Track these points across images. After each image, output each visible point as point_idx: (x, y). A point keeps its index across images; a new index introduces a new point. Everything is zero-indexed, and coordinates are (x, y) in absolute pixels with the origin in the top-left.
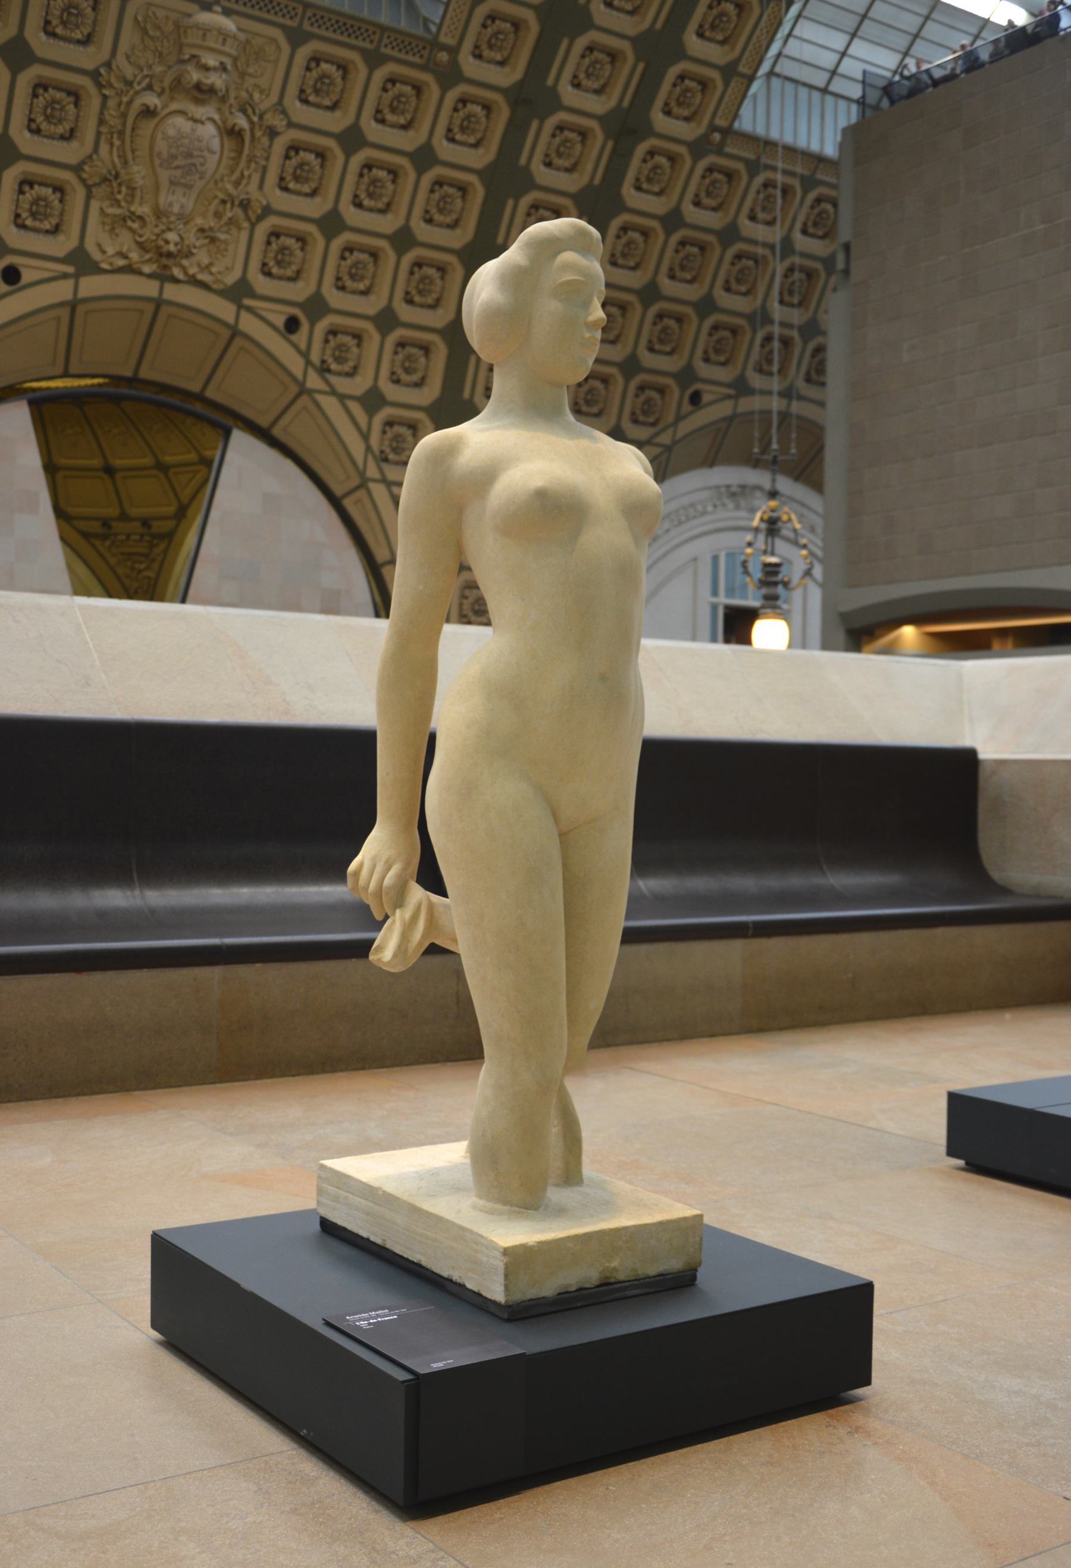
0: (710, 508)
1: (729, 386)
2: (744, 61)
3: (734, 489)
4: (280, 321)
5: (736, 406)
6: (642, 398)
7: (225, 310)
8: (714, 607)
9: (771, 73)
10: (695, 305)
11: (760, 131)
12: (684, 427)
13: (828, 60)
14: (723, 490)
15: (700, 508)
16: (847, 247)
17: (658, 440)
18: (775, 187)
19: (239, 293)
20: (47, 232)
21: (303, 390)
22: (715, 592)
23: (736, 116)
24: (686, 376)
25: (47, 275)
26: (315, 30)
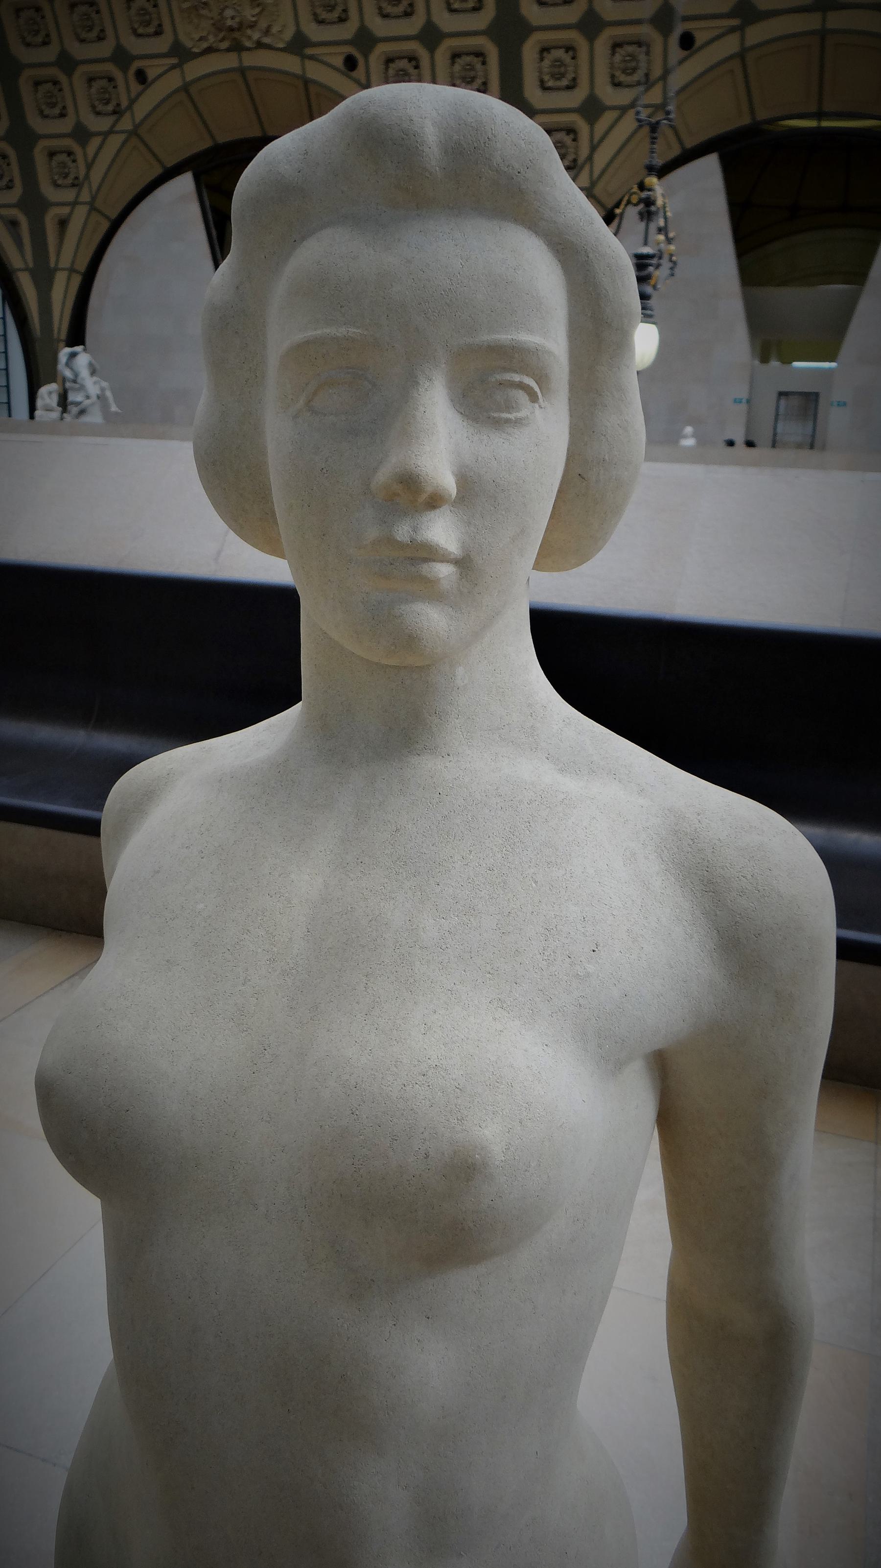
4: (339, 61)
5: (743, 39)
7: (290, 63)
12: (142, 109)
17: (118, 128)
19: (299, 45)
21: (134, 133)
24: (121, 58)
25: (716, 33)
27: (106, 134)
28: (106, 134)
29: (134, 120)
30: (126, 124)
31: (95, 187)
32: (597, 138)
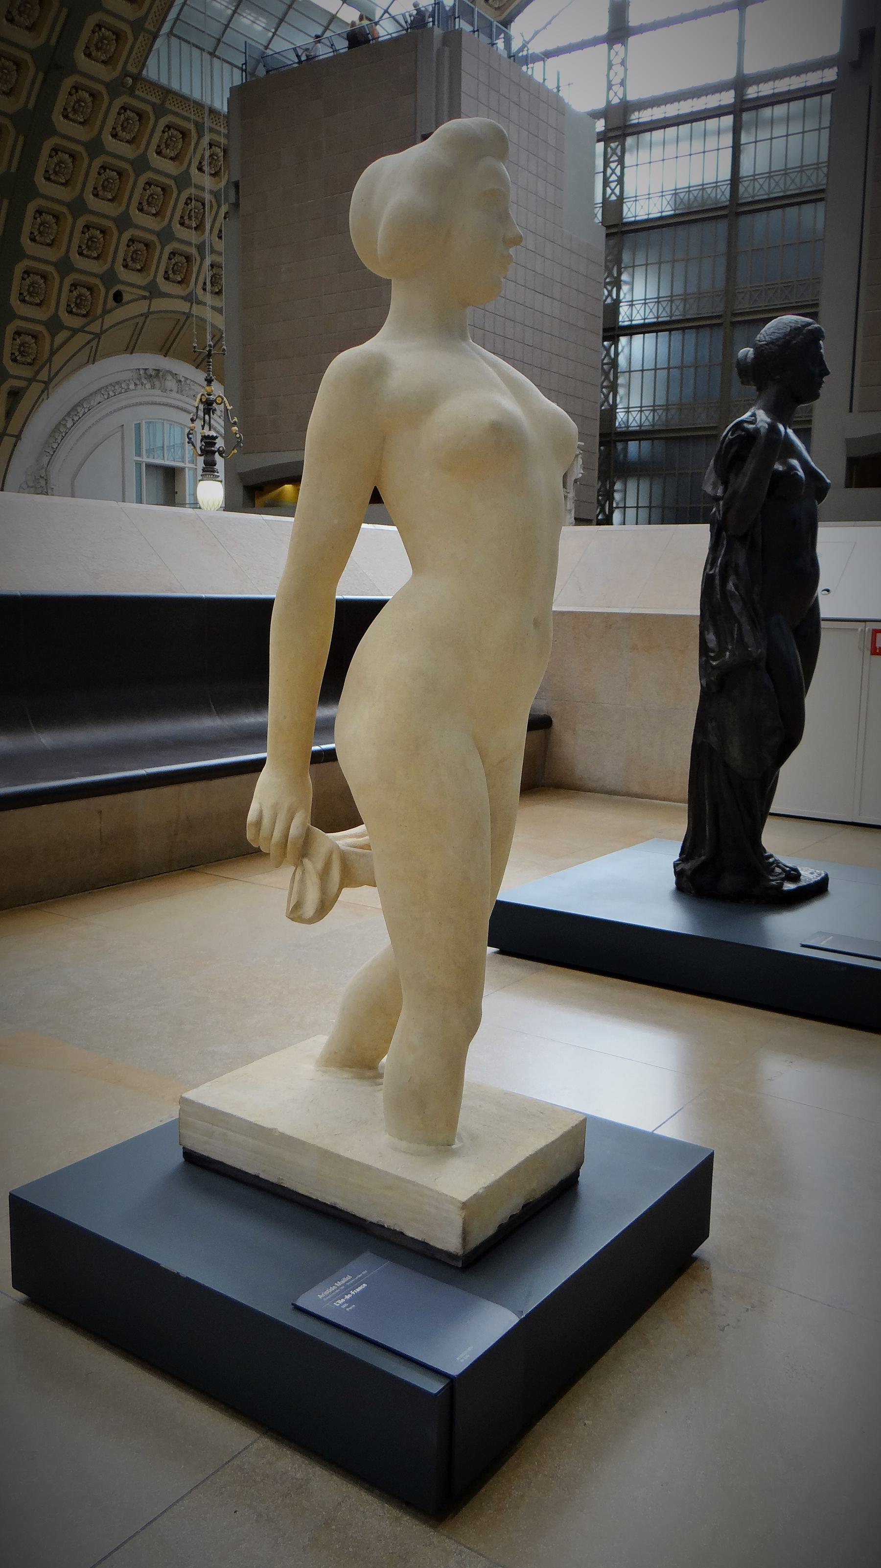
0: (132, 386)
1: (144, 288)
2: (149, 20)
6: (75, 293)
8: (138, 465)
9: (171, 33)
11: (164, 81)
12: (109, 320)
14: (142, 372)
15: (123, 385)
16: (236, 185)
20: (138, 270)
22: (139, 453)
23: (144, 65)
24: (109, 278)
25: (134, 297)
26: (173, 108)
27: (75, 331)
28: (75, 331)
29: (102, 326)
30: (95, 327)
31: (54, 370)
32: (56, 345)
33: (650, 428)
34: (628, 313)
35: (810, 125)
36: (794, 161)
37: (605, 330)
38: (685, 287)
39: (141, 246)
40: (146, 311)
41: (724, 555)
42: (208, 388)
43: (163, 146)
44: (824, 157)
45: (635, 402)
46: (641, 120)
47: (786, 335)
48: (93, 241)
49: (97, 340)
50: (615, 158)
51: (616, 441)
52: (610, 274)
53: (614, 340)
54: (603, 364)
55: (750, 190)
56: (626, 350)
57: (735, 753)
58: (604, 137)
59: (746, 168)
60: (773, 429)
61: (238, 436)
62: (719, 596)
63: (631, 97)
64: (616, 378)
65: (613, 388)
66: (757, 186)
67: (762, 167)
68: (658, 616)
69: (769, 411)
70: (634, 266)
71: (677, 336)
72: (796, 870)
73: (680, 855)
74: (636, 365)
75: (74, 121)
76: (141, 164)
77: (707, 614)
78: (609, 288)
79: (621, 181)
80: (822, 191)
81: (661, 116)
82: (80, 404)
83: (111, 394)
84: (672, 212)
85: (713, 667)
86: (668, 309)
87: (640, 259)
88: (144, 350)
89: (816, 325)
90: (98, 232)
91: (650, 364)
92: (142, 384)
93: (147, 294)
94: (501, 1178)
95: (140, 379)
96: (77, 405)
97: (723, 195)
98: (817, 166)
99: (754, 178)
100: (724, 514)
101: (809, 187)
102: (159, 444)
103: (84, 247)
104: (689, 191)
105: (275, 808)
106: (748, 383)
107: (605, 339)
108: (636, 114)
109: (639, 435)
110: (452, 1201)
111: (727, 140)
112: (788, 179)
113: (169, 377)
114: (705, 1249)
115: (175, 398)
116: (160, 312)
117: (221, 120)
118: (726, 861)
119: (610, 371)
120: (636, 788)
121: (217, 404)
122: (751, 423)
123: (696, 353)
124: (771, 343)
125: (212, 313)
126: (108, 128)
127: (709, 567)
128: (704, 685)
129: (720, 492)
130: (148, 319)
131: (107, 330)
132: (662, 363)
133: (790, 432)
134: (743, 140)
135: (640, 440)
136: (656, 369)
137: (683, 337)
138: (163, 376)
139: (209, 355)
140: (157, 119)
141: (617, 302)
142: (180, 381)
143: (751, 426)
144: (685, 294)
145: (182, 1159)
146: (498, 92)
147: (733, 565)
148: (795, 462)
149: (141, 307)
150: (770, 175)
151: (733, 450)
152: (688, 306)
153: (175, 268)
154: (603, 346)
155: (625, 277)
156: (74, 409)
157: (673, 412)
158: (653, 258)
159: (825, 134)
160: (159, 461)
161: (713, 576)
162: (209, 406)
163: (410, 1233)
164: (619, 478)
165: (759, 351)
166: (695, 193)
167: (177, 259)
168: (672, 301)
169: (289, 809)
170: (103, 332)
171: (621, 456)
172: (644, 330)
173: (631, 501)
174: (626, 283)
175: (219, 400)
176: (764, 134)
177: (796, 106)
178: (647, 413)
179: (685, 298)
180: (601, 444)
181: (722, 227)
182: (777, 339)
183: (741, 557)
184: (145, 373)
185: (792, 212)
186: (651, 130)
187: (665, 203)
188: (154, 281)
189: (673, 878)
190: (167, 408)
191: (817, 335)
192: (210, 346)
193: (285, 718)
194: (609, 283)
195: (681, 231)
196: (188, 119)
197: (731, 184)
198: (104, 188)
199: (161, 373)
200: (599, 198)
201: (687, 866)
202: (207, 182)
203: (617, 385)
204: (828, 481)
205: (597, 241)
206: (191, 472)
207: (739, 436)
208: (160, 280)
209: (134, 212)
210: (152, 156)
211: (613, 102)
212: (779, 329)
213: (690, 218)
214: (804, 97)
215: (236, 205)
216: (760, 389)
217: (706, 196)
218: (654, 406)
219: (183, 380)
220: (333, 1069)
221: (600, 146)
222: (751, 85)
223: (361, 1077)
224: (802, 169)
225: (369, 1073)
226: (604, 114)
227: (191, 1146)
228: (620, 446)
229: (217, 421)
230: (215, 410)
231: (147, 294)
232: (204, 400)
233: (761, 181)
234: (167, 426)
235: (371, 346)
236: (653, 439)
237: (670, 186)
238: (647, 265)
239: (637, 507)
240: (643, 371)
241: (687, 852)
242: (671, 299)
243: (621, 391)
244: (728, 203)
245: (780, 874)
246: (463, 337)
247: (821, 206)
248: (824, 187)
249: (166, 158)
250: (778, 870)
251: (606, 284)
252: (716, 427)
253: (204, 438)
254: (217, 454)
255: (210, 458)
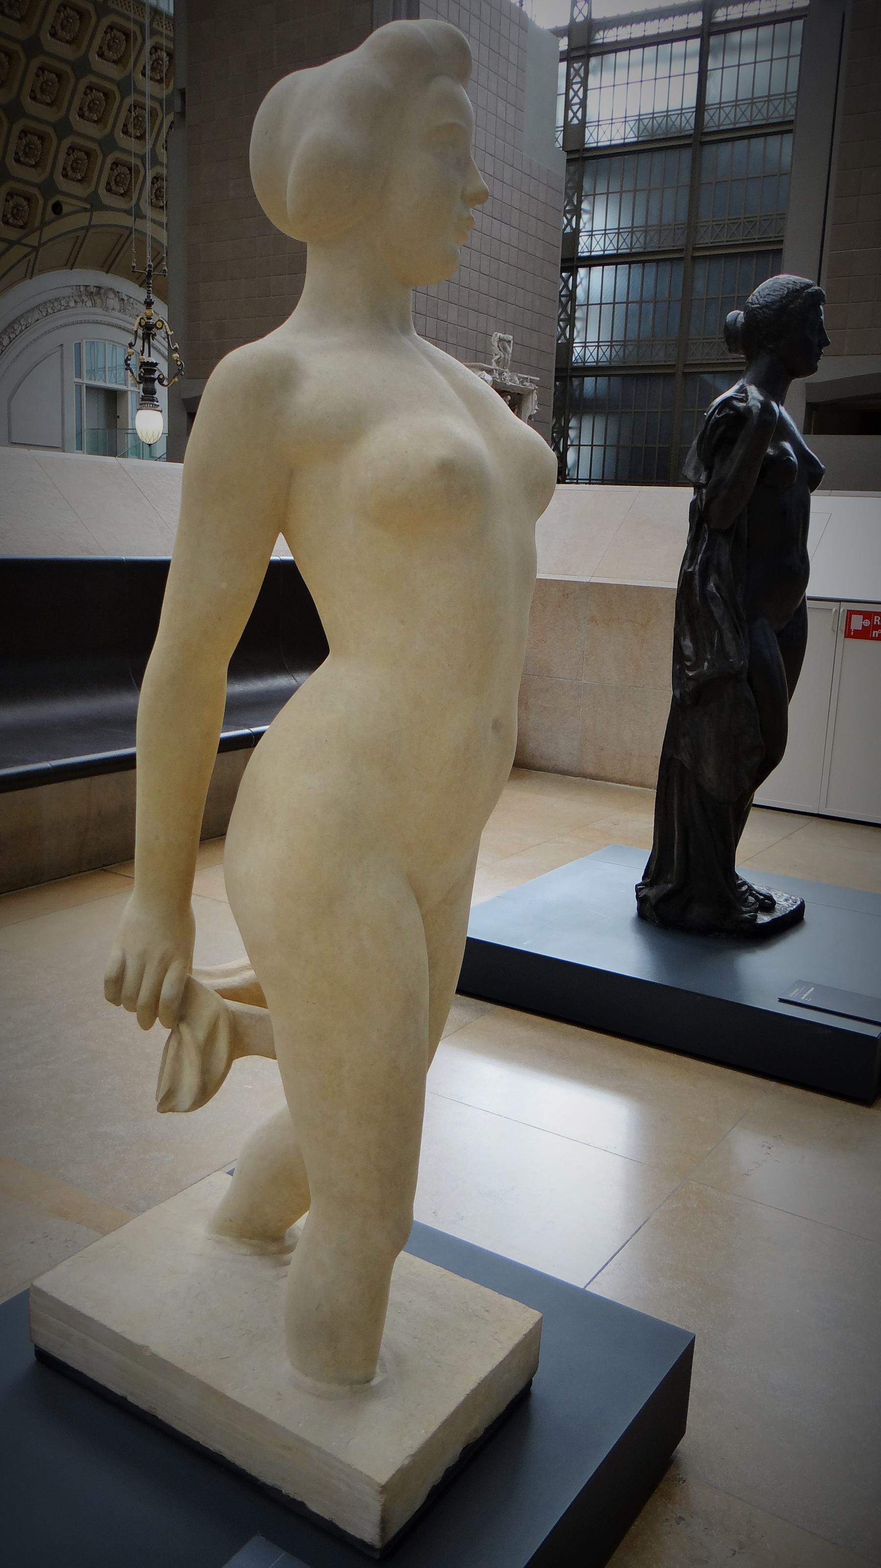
0: (72, 304)
1: (85, 200)
3: (92, 289)
8: (79, 386)
10: (100, 143)
12: (49, 232)
13: (605, 115)
14: (82, 289)
16: (183, 93)
18: (162, 50)
22: (79, 374)
24: (48, 187)
29: (40, 239)
30: (33, 240)
33: (607, 364)
34: (588, 243)
35: (780, 52)
36: (761, 91)
37: (563, 261)
38: (647, 218)
39: (82, 155)
40: (86, 224)
41: (705, 551)
42: (147, 311)
43: (105, 48)
44: (793, 86)
45: (592, 336)
46: (606, 40)
47: (783, 297)
48: (30, 148)
49: (34, 254)
50: (578, 79)
51: (571, 377)
52: (570, 202)
53: (574, 273)
54: (561, 296)
55: (716, 118)
56: (585, 282)
57: (710, 774)
58: (568, 57)
59: (712, 95)
60: (766, 408)
61: (179, 363)
62: (698, 598)
63: (596, 16)
64: (574, 311)
65: (571, 321)
66: (723, 115)
67: (729, 95)
68: (619, 586)
69: (760, 386)
70: (594, 195)
71: (636, 269)
72: (770, 898)
73: (644, 878)
74: (595, 298)
75: (10, 17)
76: (82, 67)
77: (684, 618)
78: (569, 216)
79: (583, 104)
80: (791, 122)
81: (627, 37)
82: (17, 320)
83: (50, 311)
84: (635, 139)
85: (689, 678)
86: (628, 241)
87: (601, 188)
88: (85, 266)
89: (817, 288)
90: (36, 138)
91: (608, 298)
92: (83, 301)
93: (88, 206)
94: (434, 1435)
95: (80, 296)
96: (14, 322)
97: (688, 123)
98: (785, 96)
99: (720, 106)
100: (707, 505)
101: (776, 118)
102: (101, 365)
103: (21, 154)
104: (653, 118)
105: (143, 958)
106: (737, 351)
107: (563, 270)
108: (601, 33)
109: (596, 371)
110: (369, 1481)
111: (694, 65)
112: (754, 108)
113: (112, 295)
114: (684, 1445)
115: (116, 317)
116: (102, 226)
117: (163, 20)
118: (694, 892)
119: (567, 303)
120: (590, 769)
121: (158, 328)
122: (741, 400)
123: (656, 287)
124: (766, 306)
125: (154, 228)
126: (47, 26)
127: (687, 563)
128: (678, 696)
129: (703, 479)
130: (89, 234)
131: (44, 244)
132: (621, 296)
133: (782, 409)
134: (711, 65)
135: (596, 376)
136: (614, 303)
137: (643, 269)
138: (105, 294)
139: (149, 275)
140: (99, 18)
141: (576, 232)
142: (123, 300)
143: (741, 405)
144: (646, 226)
145: (34, 1358)
146: (459, 4)
147: (715, 563)
148: (787, 446)
149: (82, 219)
150: (736, 103)
151: (719, 431)
152: (648, 239)
153: (118, 179)
154: (561, 276)
155: (585, 206)
156: (11, 325)
157: (631, 348)
158: (615, 186)
159: (795, 63)
160: (100, 383)
161: (692, 574)
162: (148, 331)
163: (314, 1507)
164: (574, 415)
165: (751, 315)
166: (660, 120)
167: (120, 169)
168: (632, 233)
169: (162, 959)
170: (41, 245)
171: (577, 393)
172: (603, 262)
173: (586, 439)
174: (586, 212)
175: (159, 325)
176: (731, 60)
177: (765, 32)
178: (604, 348)
179: (646, 229)
180: (557, 379)
181: (686, 156)
182: (773, 303)
183: (724, 554)
184: (86, 290)
185: (758, 144)
186: (616, 51)
187: (628, 129)
188: (96, 192)
189: (635, 903)
190: (109, 328)
191: (817, 298)
192: (150, 266)
193: (157, 838)
194: (569, 212)
195: (644, 159)
196: (128, 18)
197: (696, 111)
198: (42, 91)
199: (103, 291)
200: (560, 122)
201: (652, 893)
202: (148, 86)
203: (575, 318)
204: (823, 466)
205: (557, 165)
206: (134, 396)
207: (727, 414)
208: (102, 192)
209: (74, 117)
210: (94, 58)
211: (577, 20)
212: (774, 291)
213: (655, 145)
214: (774, 23)
215: (182, 114)
216: (750, 358)
217: (670, 123)
218: (611, 341)
219: (125, 298)
220: (228, 1239)
221: (563, 66)
222: (720, 7)
223: (262, 1253)
224: (769, 98)
225: (273, 1247)
226: (569, 31)
227: (43, 1345)
228: (576, 382)
229: (160, 341)
230: (155, 335)
231: (88, 206)
232: (143, 323)
233: (727, 110)
234: (109, 347)
235: (275, 342)
236: (609, 376)
237: (633, 112)
238: (608, 193)
239: (592, 446)
240: (601, 304)
241: (652, 875)
242: (632, 231)
243: (579, 325)
244: (692, 132)
245: (753, 904)
246: (404, 329)
247: (788, 139)
248: (793, 118)
249: (108, 61)
250: (751, 899)
251: (566, 212)
252: (674, 365)
253: (143, 364)
254: (157, 382)
255: (149, 386)
